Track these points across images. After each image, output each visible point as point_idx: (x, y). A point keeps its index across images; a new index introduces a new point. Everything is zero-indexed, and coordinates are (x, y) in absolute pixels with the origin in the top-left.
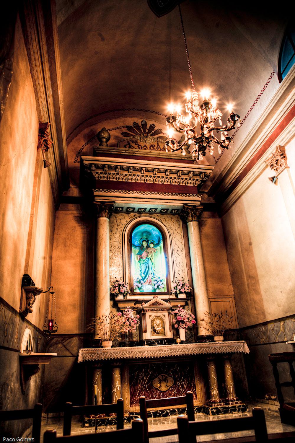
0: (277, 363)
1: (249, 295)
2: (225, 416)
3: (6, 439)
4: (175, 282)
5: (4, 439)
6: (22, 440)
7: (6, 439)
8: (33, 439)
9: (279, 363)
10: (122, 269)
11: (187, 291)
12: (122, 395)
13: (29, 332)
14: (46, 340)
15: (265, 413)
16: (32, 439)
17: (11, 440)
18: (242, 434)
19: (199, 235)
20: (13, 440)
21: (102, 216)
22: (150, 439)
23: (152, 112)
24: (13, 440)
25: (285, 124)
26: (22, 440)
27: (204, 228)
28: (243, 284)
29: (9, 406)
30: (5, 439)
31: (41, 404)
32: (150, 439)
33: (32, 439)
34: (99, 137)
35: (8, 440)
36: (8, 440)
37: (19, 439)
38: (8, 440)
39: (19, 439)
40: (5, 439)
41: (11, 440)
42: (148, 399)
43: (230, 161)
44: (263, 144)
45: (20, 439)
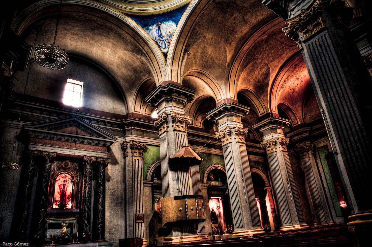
1: (118, 197)
3: (5, 244)
5: (3, 244)
6: (18, 244)
7: (5, 244)
8: (28, 243)
12: (302, 46)
16: (27, 244)
17: (9, 244)
19: (123, 177)
20: (11, 244)
23: (57, 29)
24: (11, 244)
25: (125, 162)
26: (18, 244)
27: (88, 77)
30: (4, 243)
31: (55, 206)
33: (27, 244)
35: (7, 244)
36: (7, 244)
38: (7, 244)
39: (16, 243)
40: (4, 243)
41: (9, 244)
43: (133, 231)
44: (116, 16)
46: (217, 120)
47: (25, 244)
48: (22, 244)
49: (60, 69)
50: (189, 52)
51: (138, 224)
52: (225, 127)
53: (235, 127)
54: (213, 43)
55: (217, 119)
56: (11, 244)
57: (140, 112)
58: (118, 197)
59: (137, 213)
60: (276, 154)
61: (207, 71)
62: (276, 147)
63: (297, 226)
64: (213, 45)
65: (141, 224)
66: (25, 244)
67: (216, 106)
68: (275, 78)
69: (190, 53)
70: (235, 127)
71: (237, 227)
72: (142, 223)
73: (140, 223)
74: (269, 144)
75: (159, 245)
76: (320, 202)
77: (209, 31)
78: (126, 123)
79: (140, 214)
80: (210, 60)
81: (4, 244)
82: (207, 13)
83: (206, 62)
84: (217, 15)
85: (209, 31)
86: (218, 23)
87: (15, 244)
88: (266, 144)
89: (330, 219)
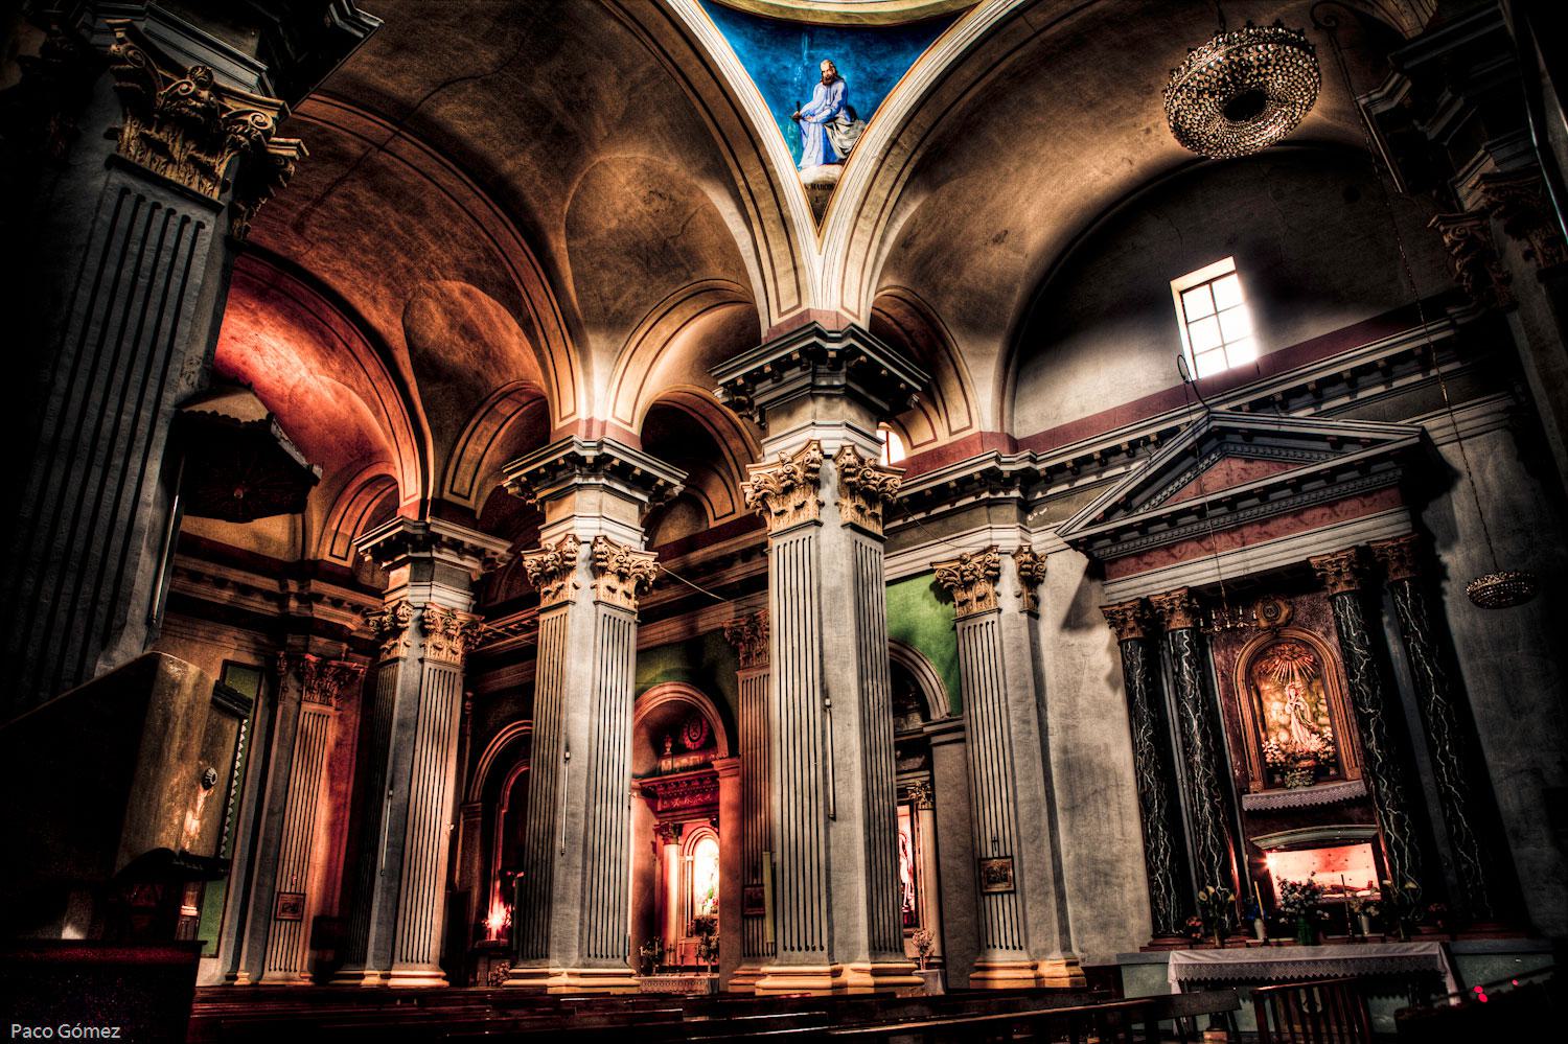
0: (39, 56)
2: (1064, 809)
3: (22, 1031)
4: (959, 735)
5: (14, 1031)
6: (77, 1033)
7: (22, 1031)
8: (118, 1029)
9: (1175, 385)
11: (697, 216)
17: (39, 1033)
20: (48, 1033)
24: (48, 1033)
26: (77, 1033)
29: (137, 612)
30: (16, 1028)
31: (15, 1028)
33: (113, 1032)
34: (1102, 716)
35: (28, 1033)
36: (28, 1033)
37: (66, 1028)
38: (29, 1032)
39: (66, 1028)
40: (16, 1028)
41: (39, 1033)
46: (543, 501)
47: (105, 1033)
48: (91, 1031)
49: (53, 123)
51: (993, 897)
53: (600, 540)
55: (540, 495)
56: (47, 1032)
60: (996, 620)
62: (996, 589)
63: (855, 970)
65: (1000, 897)
66: (105, 1033)
67: (547, 441)
70: (600, 540)
71: (1007, 948)
72: (1012, 896)
74: (971, 573)
75: (1254, 1021)
76: (273, 922)
78: (1399, 104)
88: (956, 569)
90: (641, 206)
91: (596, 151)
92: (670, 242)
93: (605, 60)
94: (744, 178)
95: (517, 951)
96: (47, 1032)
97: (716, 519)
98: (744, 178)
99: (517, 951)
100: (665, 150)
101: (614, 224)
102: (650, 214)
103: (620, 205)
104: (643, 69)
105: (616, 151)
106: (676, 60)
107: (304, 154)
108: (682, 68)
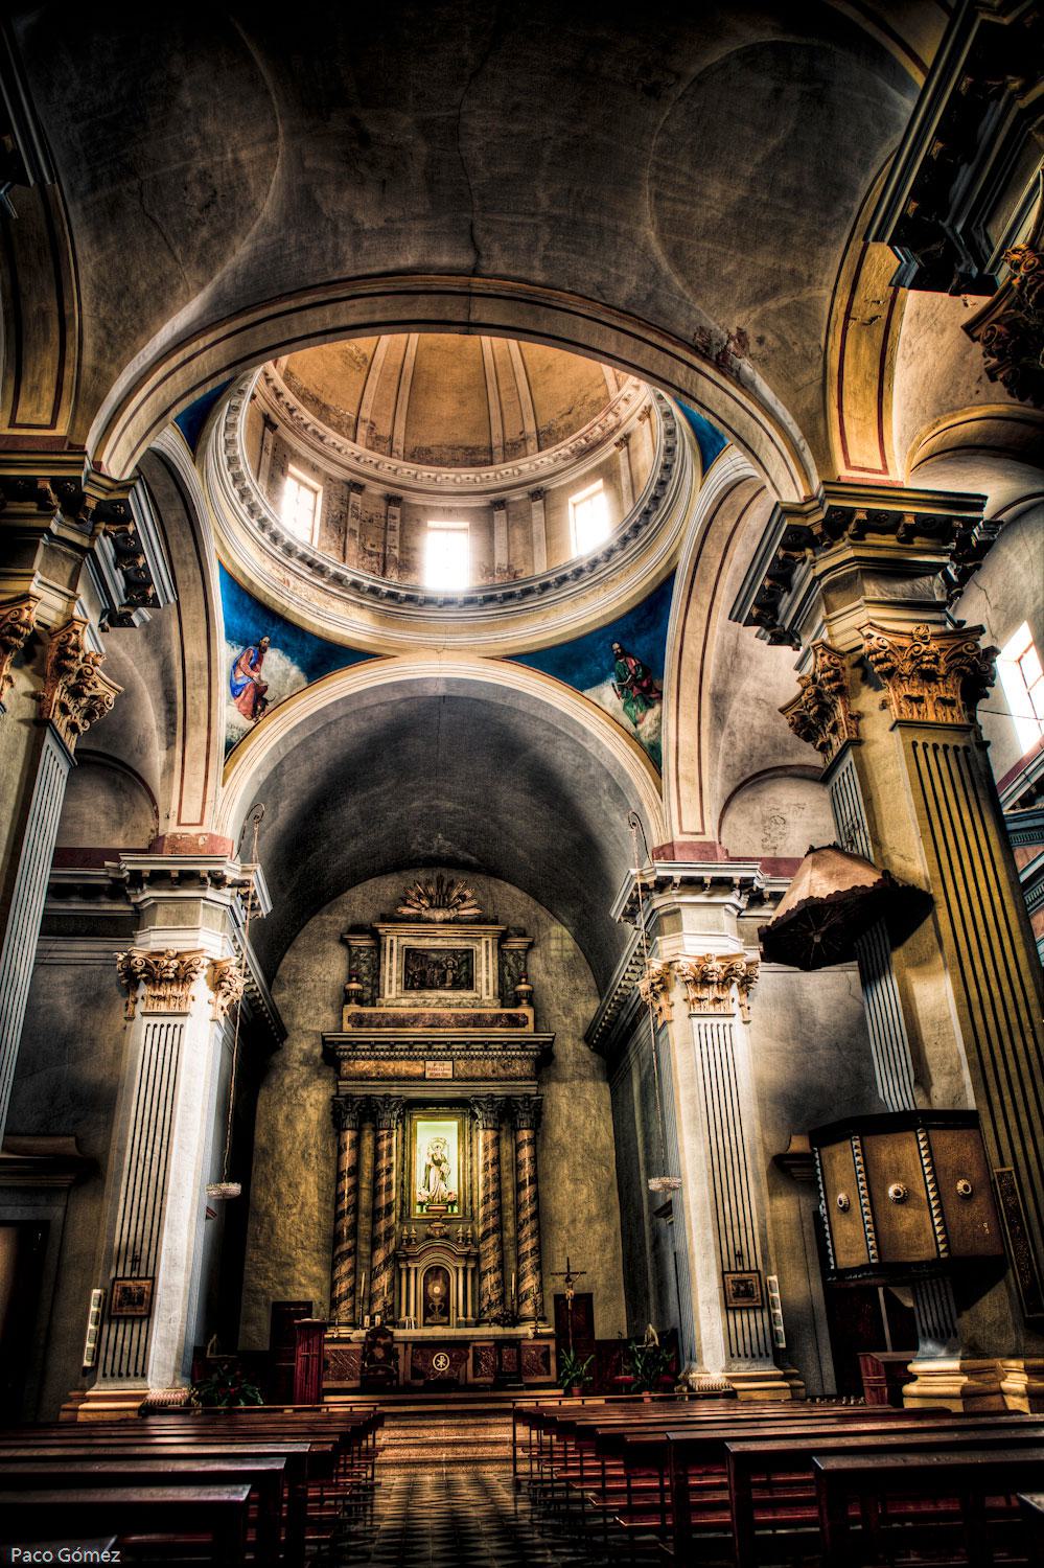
3: (22, 1555)
5: (14, 1556)
7: (22, 1555)
10: (741, 525)
13: (212, 1029)
14: (641, 744)
15: (959, 1107)
17: (39, 1556)
18: (48, 389)
21: (410, 1346)
22: (598, 1337)
24: (48, 1556)
26: (77, 1556)
28: (313, 924)
30: (17, 1552)
32: (598, 1337)
33: (113, 1555)
36: (28, 1557)
40: (17, 1552)
41: (39, 1556)
42: (645, 1263)
45: (71, 1553)
50: (731, 338)
52: (445, 609)
54: (681, 180)
57: (703, 833)
58: (794, 1248)
59: (733, 1269)
61: (854, 192)
64: (690, 178)
68: (212, 330)
69: (734, 332)
73: (747, 1308)
77: (624, 226)
79: (744, 1272)
80: (786, 178)
81: (15, 1553)
82: (544, 268)
83: (796, 194)
84: (533, 215)
85: (624, 226)
86: (570, 190)
87: (63, 1557)
89: (46, 331)
90: (200, 163)
91: (292, 134)
92: (135, 184)
93: (382, 223)
94: (205, 349)
95: (94, 1368)
96: (47, 1556)
97: (179, 824)
98: (205, 349)
99: (94, 1368)
100: (261, 241)
101: (187, 99)
102: (186, 170)
103: (210, 126)
104: (350, 255)
105: (283, 172)
106: (343, 305)
107: (809, 1482)
108: (333, 306)
